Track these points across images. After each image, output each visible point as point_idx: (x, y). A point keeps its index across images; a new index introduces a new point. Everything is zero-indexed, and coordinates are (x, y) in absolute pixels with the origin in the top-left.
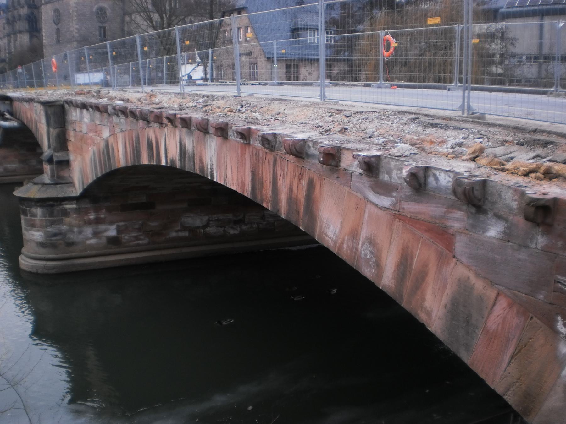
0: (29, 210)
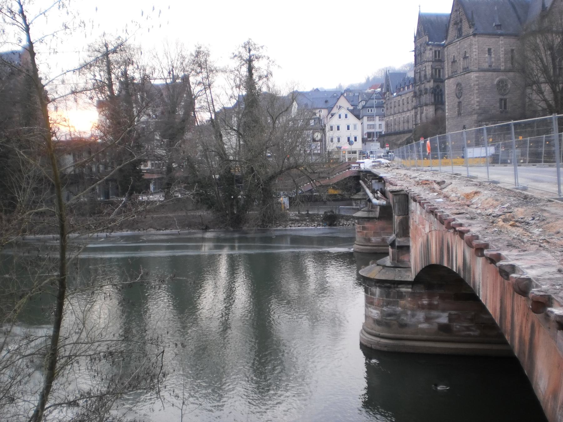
0: (370, 289)
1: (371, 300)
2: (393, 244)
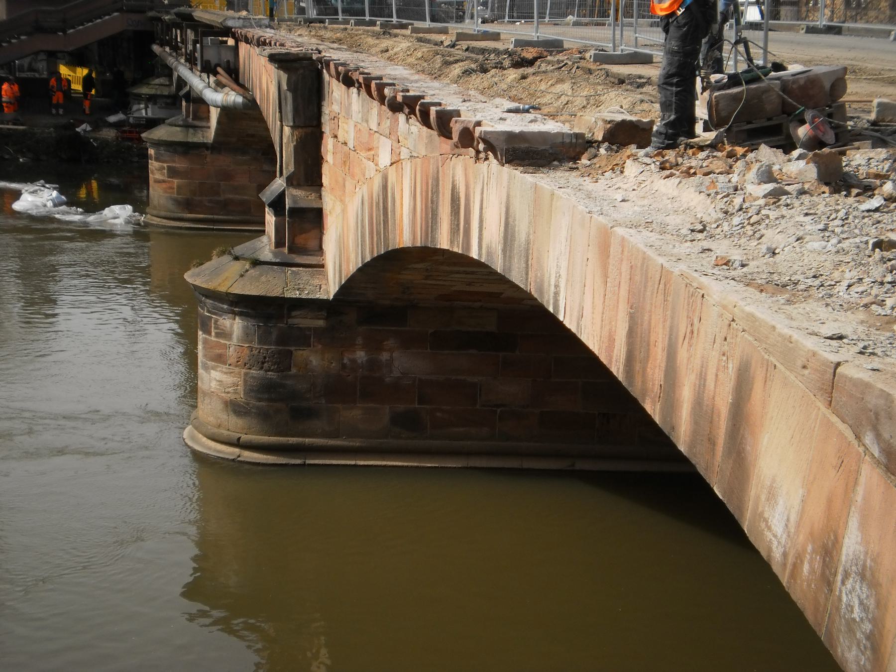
0: (216, 321)
1: (218, 351)
2: (278, 204)
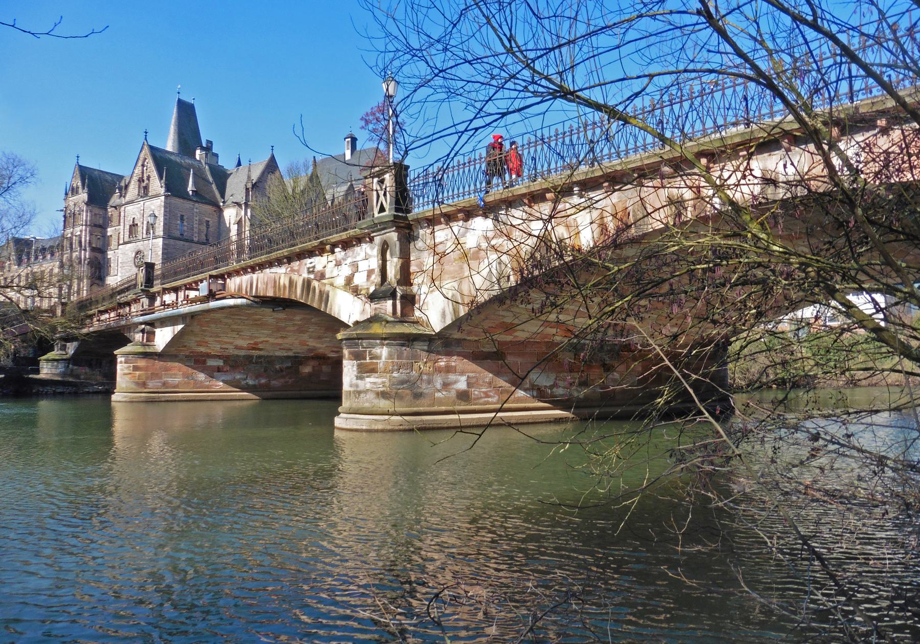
0: (370, 352)
